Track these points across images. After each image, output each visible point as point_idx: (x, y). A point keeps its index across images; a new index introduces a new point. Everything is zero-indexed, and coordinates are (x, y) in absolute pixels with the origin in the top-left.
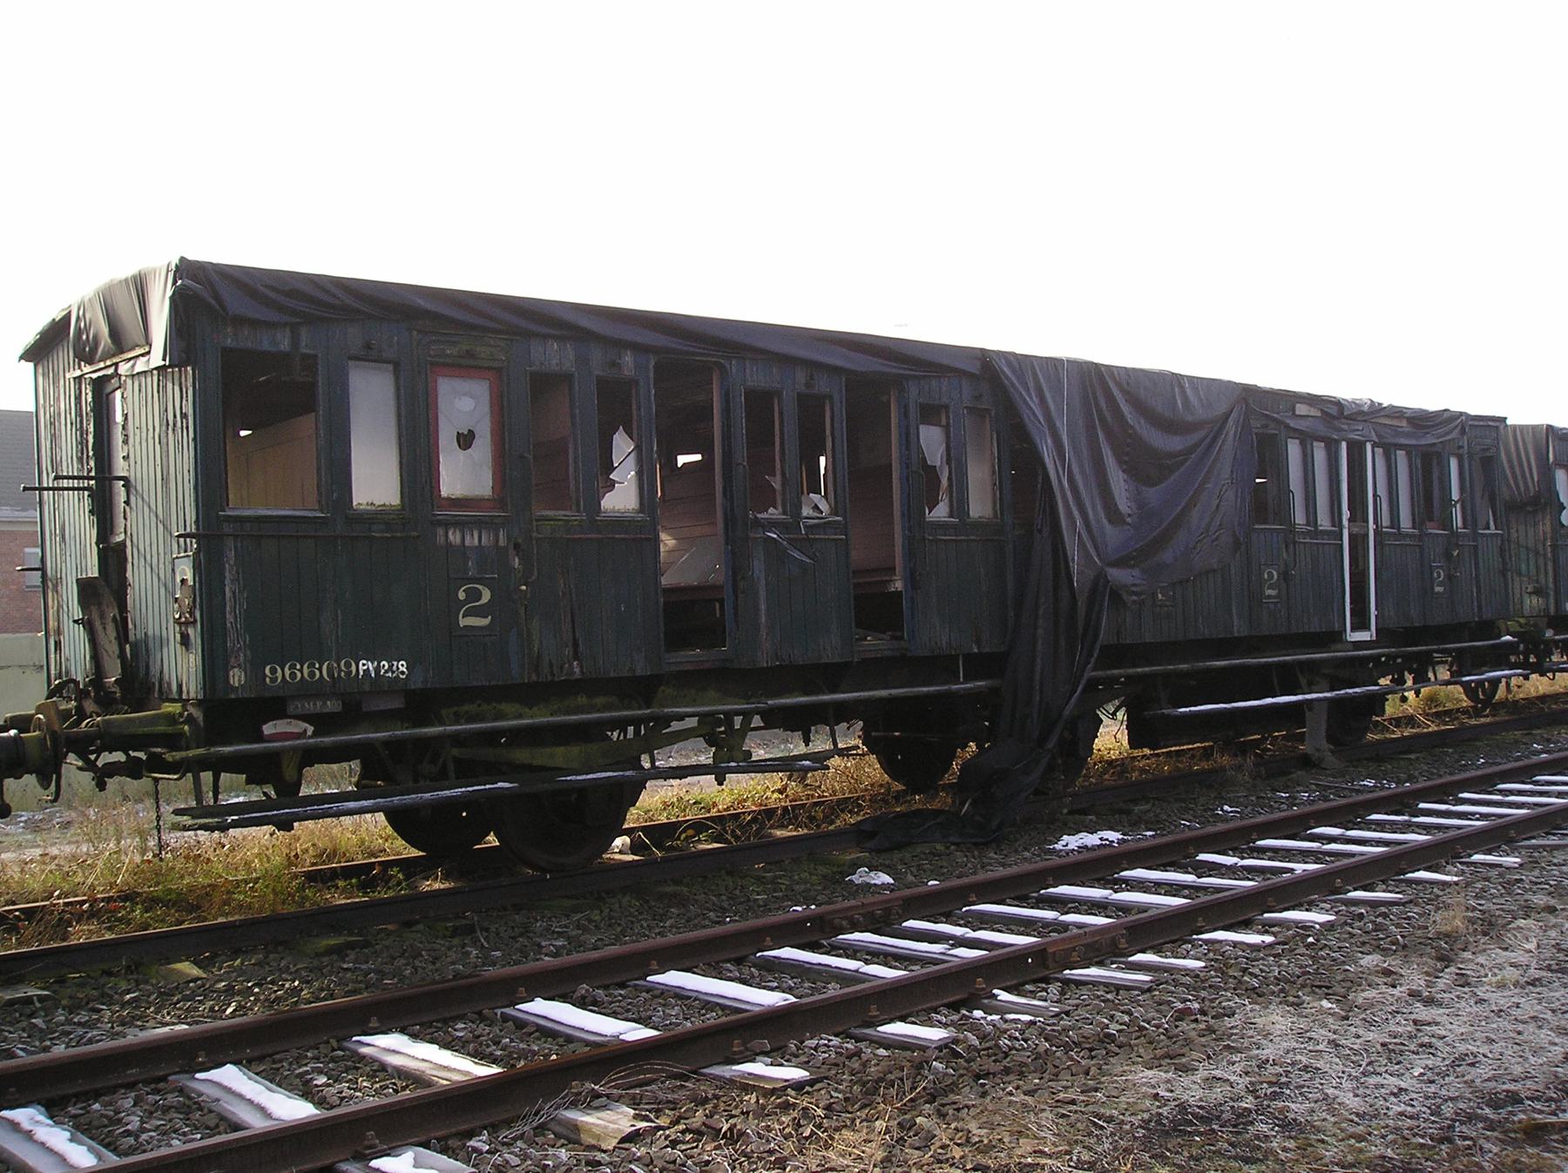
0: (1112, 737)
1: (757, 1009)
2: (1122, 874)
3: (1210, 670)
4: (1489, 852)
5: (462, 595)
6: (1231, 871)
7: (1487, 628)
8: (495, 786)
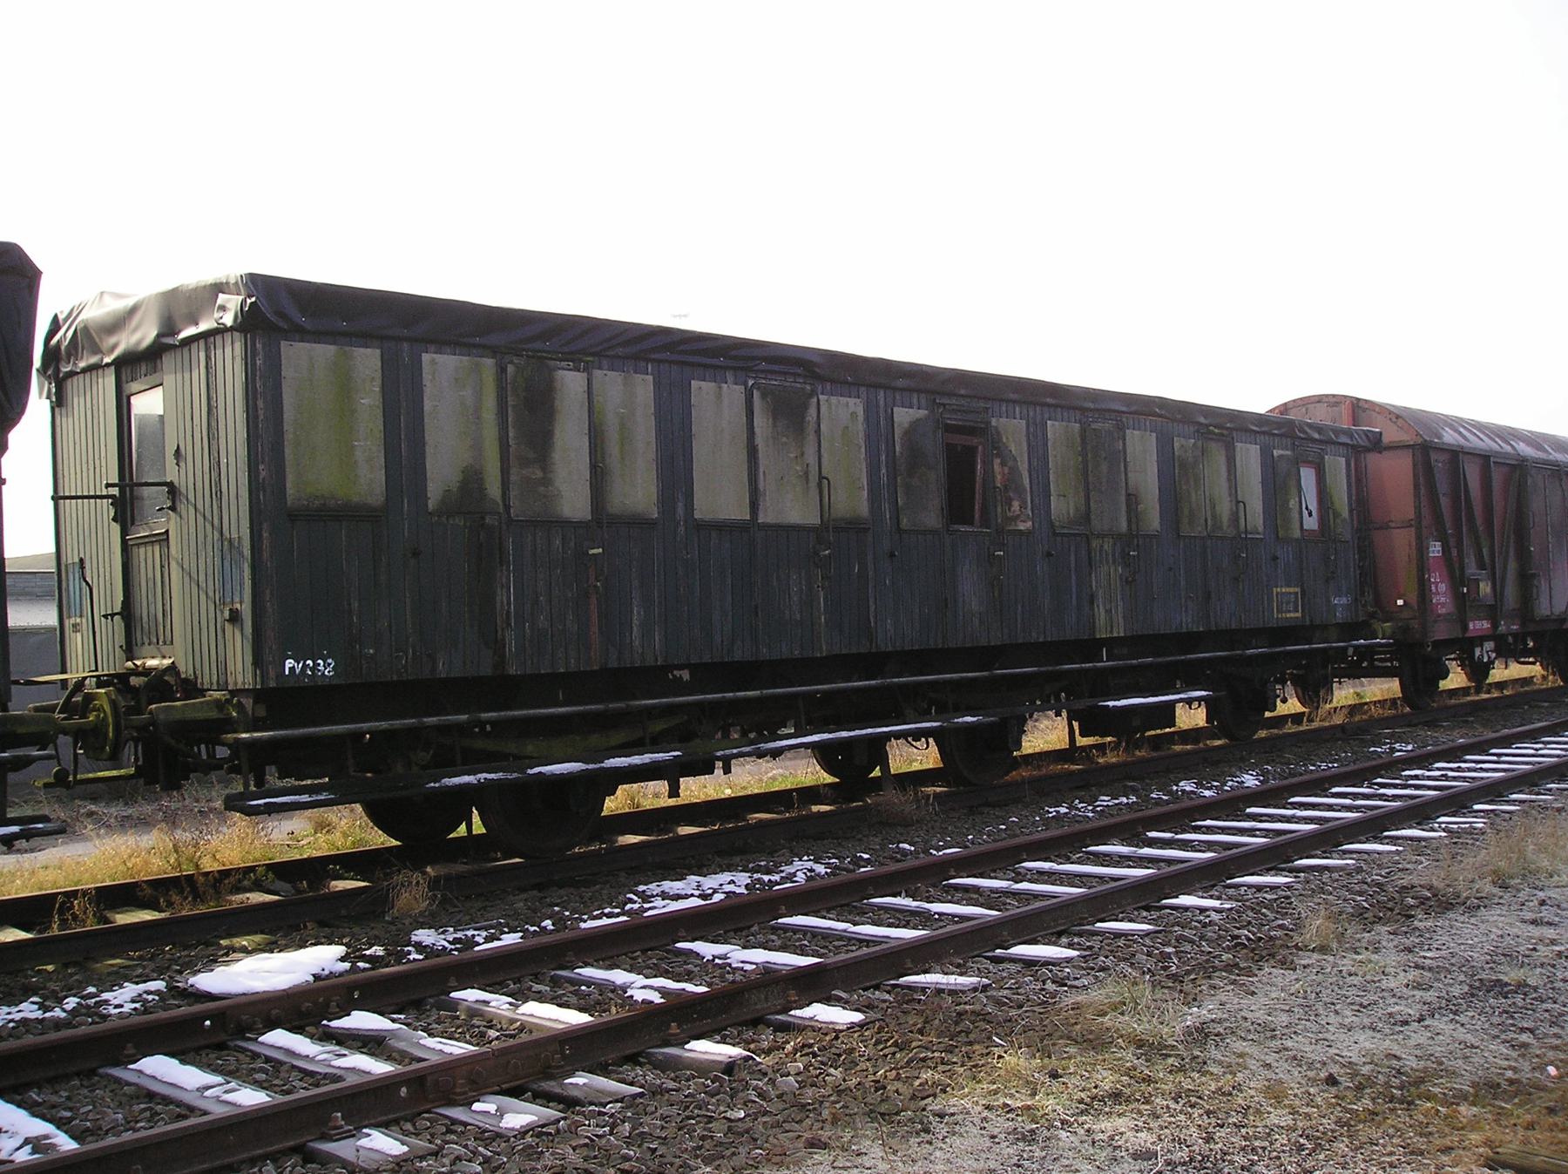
1: (561, 1026)
2: (780, 921)
6: (1121, 861)
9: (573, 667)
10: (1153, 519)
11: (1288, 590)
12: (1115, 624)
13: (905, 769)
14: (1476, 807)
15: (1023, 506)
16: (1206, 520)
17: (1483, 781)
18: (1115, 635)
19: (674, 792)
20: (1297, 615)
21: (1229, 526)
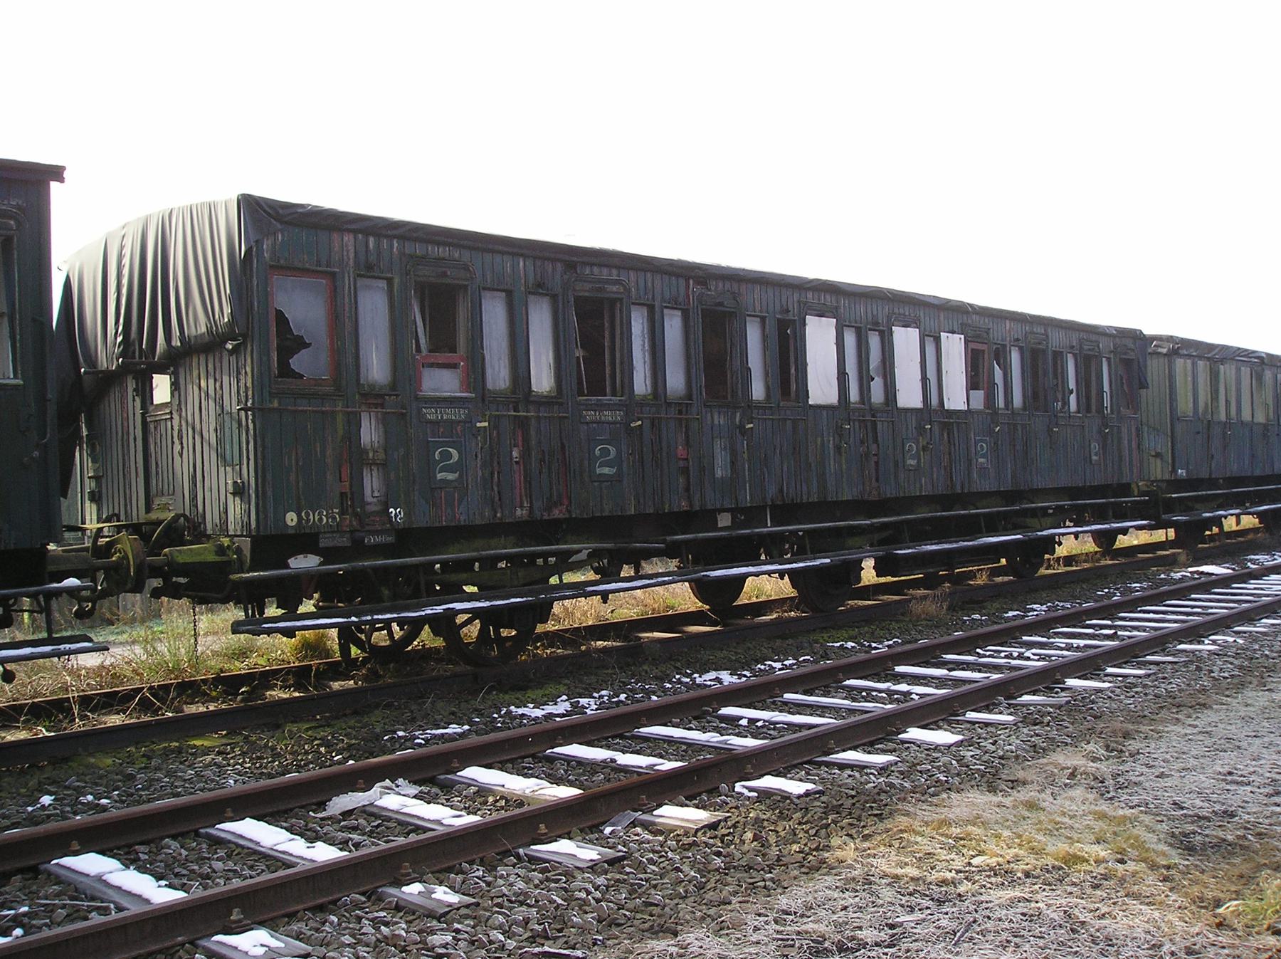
0: (869, 574)
3: (677, 540)
4: (1191, 642)
5: (597, 452)
7: (706, 518)
8: (349, 620)
9: (1044, 487)
13: (1229, 530)
14: (1110, 670)
17: (1215, 616)
19: (1238, 523)
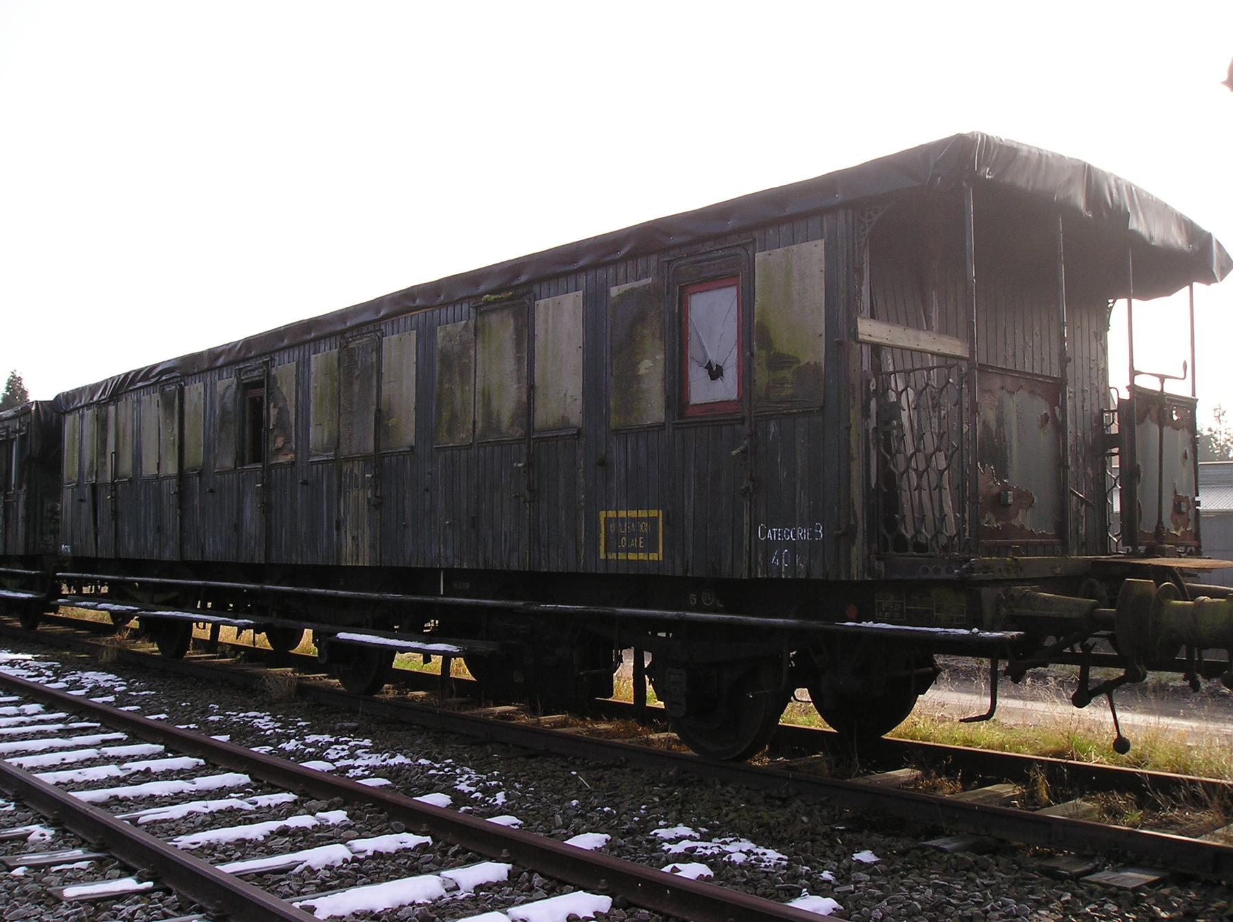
10: (406, 432)
11: (633, 514)
12: (361, 554)
15: (287, 441)
16: (474, 422)
18: (361, 564)
20: (653, 557)
21: (512, 425)
